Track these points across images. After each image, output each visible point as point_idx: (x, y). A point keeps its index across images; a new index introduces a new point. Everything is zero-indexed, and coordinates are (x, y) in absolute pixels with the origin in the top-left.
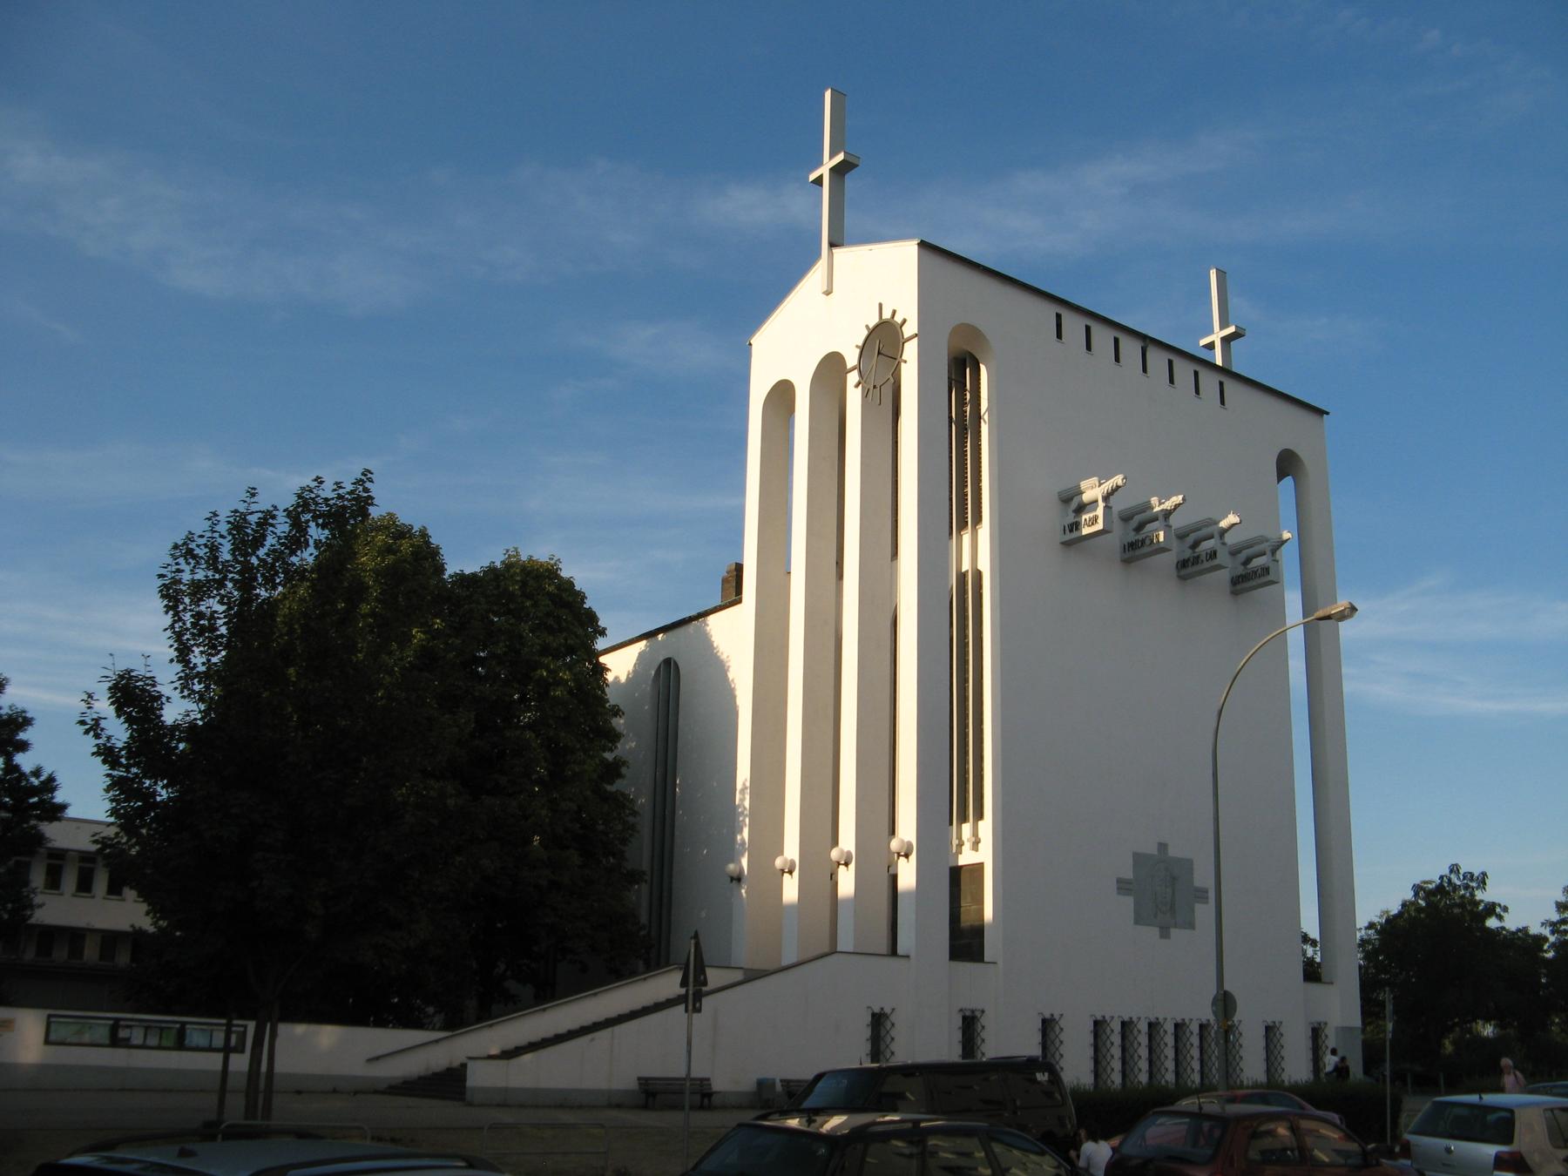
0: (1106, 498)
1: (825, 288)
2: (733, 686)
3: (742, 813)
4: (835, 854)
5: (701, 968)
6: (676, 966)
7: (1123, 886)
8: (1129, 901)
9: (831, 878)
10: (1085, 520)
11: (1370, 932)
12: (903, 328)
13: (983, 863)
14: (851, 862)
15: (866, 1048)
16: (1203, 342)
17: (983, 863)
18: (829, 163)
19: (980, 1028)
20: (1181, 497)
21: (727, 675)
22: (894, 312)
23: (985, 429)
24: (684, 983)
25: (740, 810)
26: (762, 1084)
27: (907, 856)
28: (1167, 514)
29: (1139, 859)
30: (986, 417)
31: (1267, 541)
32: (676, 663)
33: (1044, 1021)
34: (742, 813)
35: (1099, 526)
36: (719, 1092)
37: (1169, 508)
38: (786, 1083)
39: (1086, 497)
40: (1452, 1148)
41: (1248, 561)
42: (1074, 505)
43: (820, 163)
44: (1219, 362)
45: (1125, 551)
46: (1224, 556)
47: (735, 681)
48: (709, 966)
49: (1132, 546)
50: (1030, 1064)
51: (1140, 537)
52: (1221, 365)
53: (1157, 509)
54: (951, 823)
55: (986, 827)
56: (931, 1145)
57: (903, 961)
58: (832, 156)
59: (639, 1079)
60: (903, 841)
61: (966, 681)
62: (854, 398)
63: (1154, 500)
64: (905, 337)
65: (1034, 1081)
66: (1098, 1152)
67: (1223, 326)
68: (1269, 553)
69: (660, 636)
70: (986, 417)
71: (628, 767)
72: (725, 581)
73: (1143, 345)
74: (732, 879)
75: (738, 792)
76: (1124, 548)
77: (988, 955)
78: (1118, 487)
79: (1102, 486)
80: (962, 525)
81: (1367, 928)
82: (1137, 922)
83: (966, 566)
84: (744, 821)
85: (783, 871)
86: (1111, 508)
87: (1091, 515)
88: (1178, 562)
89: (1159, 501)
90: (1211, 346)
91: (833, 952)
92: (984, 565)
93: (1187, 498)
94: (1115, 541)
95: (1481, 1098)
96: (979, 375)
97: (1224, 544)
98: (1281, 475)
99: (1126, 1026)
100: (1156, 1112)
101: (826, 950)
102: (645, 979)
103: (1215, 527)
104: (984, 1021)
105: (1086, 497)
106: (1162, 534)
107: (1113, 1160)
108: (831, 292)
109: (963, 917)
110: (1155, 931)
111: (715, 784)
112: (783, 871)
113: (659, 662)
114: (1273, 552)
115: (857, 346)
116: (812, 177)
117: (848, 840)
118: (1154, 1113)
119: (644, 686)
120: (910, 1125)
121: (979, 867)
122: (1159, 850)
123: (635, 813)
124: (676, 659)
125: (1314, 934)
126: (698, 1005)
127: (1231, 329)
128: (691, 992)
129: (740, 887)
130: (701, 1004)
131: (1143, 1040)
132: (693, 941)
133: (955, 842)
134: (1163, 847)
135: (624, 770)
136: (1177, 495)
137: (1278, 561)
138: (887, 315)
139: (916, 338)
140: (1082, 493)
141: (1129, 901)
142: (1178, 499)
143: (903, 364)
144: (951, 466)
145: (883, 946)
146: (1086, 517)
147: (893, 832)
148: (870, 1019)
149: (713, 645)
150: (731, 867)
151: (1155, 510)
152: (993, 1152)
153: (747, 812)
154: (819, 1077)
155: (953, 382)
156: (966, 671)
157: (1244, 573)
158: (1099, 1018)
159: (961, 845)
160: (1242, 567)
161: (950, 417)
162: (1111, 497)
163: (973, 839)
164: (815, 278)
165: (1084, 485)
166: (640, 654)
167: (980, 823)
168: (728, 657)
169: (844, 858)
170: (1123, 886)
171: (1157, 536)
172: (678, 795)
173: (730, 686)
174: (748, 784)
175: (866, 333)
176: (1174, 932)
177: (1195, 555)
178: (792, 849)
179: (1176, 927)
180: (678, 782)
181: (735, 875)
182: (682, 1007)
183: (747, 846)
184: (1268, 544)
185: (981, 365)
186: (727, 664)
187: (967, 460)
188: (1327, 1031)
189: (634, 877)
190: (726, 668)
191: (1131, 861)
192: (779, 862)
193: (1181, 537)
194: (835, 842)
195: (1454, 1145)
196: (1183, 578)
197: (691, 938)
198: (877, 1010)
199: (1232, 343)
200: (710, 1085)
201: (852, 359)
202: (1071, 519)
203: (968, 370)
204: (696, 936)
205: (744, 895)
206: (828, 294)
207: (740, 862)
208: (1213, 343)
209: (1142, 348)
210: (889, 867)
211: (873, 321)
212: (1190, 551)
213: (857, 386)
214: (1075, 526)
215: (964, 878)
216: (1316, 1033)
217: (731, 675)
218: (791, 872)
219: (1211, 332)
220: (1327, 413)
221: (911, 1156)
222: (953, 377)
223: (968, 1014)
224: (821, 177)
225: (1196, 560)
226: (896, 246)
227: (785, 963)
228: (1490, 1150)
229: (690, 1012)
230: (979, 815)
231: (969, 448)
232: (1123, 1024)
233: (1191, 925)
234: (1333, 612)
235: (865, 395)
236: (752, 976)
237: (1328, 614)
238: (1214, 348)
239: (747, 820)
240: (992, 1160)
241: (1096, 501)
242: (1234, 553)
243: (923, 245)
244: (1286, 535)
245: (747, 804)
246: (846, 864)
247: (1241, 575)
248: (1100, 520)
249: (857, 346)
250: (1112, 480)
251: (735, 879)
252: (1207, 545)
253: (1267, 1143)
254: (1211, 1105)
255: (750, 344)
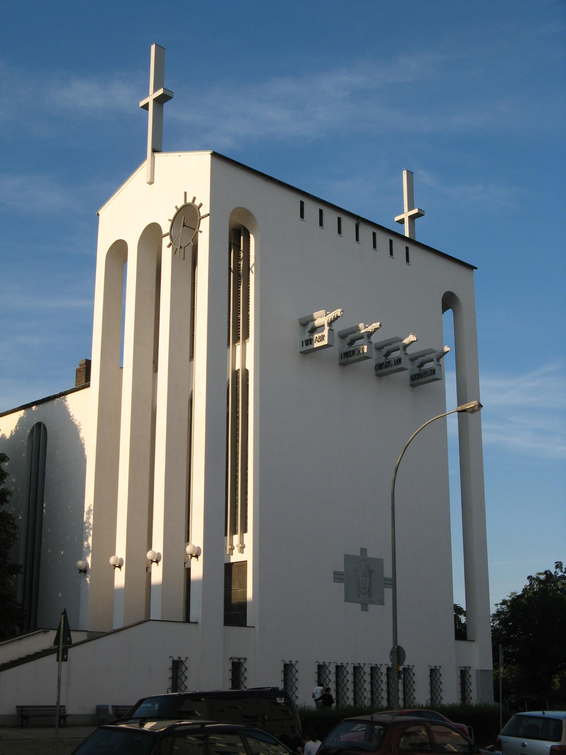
0: (330, 324)
1: (149, 180)
2: (83, 442)
3: (88, 527)
4: (149, 555)
5: (68, 632)
6: (41, 630)
7: (338, 577)
8: (341, 586)
9: (147, 571)
10: (316, 337)
11: (503, 606)
12: (200, 209)
13: (246, 561)
14: (160, 560)
15: (169, 684)
16: (397, 218)
17: (246, 561)
18: (153, 95)
19: (243, 670)
20: (378, 324)
21: (79, 435)
22: (194, 199)
23: (252, 277)
24: (57, 642)
25: (87, 525)
26: (100, 709)
27: (197, 556)
28: (369, 334)
29: (347, 558)
30: (253, 269)
31: (434, 352)
32: (44, 426)
33: (286, 665)
34: (88, 527)
35: (325, 342)
36: (71, 715)
37: (371, 331)
38: (115, 708)
39: (317, 323)
40: (526, 743)
41: (422, 364)
42: (309, 327)
43: (147, 95)
44: (407, 235)
45: (342, 358)
46: (405, 363)
47: (84, 439)
48: (72, 630)
49: (347, 355)
50: (274, 692)
51: (351, 349)
52: (408, 236)
53: (363, 331)
54: (226, 535)
55: (249, 537)
56: (211, 739)
57: (194, 626)
58: (155, 90)
59: (17, 707)
60: (194, 546)
61: (237, 441)
62: (167, 254)
63: (361, 325)
64: (201, 215)
65: (276, 703)
66: (313, 746)
67: (410, 209)
68: (435, 360)
69: (34, 407)
70: (253, 269)
71: (11, 496)
72: (78, 371)
73: (357, 223)
74: (81, 571)
75: (85, 513)
76: (341, 356)
77: (249, 623)
78: (338, 317)
79: (328, 316)
80: (237, 339)
81: (501, 604)
82: (346, 600)
83: (238, 366)
84: (89, 532)
85: (115, 566)
86: (333, 330)
87: (320, 335)
88: (376, 365)
89: (365, 326)
90: (402, 222)
91: (148, 620)
92: (250, 366)
93: (382, 324)
94: (335, 351)
95: (544, 713)
96: (249, 241)
97: (406, 354)
98: (445, 309)
99: (357, 669)
100: (346, 720)
101: (143, 619)
102: (21, 639)
103: (399, 343)
104: (246, 665)
105: (317, 323)
106: (366, 347)
107: (320, 749)
108: (153, 183)
109: (233, 597)
110: (359, 606)
111: (70, 507)
112: (115, 566)
113: (33, 425)
114: (438, 360)
115: (169, 220)
116: (142, 103)
117: (158, 546)
118: (345, 721)
119: (22, 441)
120: (199, 726)
121: (244, 564)
122: (361, 554)
123: (15, 527)
124: (44, 423)
125: (464, 606)
126: (65, 656)
127: (415, 211)
128: (61, 648)
129: (86, 577)
130: (67, 656)
131: (367, 678)
132: (63, 616)
133: (228, 547)
134: (364, 551)
135: (8, 498)
136: (376, 322)
137: (441, 365)
138: (189, 200)
139: (209, 217)
140: (314, 320)
141: (341, 586)
142: (376, 325)
143: (199, 233)
144: (230, 300)
145: (181, 618)
146: (316, 335)
147: (188, 540)
148: (171, 664)
149: (70, 415)
150: (80, 563)
151: (362, 332)
152: (248, 743)
153: (91, 527)
154: (141, 702)
155: (232, 245)
156: (237, 435)
157: (419, 373)
158: (288, 662)
159: (232, 549)
160: (418, 369)
161: (230, 268)
162: (333, 323)
163: (240, 545)
164: (142, 172)
165: (316, 315)
166: (20, 419)
167: (245, 534)
168: (80, 423)
169: (156, 558)
170: (338, 577)
171: (363, 349)
172: (44, 514)
173: (81, 442)
174: (92, 508)
175: (175, 211)
176: (370, 607)
177: (387, 361)
178: (121, 552)
179: (372, 603)
180: (44, 506)
181: (83, 568)
182: (55, 656)
183: (91, 549)
184: (434, 354)
185: (250, 234)
186: (79, 428)
187: (239, 323)
188: (470, 673)
189: (14, 569)
190: (78, 430)
191: (342, 562)
192: (112, 560)
193: (379, 348)
194: (150, 547)
195: (527, 741)
196: (379, 376)
197: (62, 614)
198: (176, 659)
199: (415, 220)
200: (65, 710)
201: (166, 228)
202: (307, 337)
203: (242, 237)
204: (65, 613)
205: (89, 582)
206: (150, 184)
207: (86, 560)
208: (403, 219)
209: (356, 224)
210: (185, 563)
211: (181, 204)
212: (384, 358)
213: (169, 246)
214: (310, 342)
215: (234, 570)
216: (464, 674)
217: (81, 435)
218: (120, 567)
219: (402, 212)
220: (476, 268)
221: (200, 745)
222: (232, 242)
223: (236, 660)
224: (147, 105)
225: (388, 364)
226: (197, 155)
227: (115, 627)
228: (548, 744)
229: (60, 661)
230: (245, 530)
231: (241, 289)
232: (337, 667)
233: (382, 603)
234: (467, 407)
235: (174, 253)
236: (94, 636)
237: (464, 409)
238: (404, 223)
239: (91, 532)
240: (247, 748)
241: (324, 326)
242: (413, 359)
243: (214, 155)
244: (446, 349)
245: (91, 521)
246: (157, 562)
247: (417, 374)
248: (326, 338)
249: (169, 220)
250: (334, 312)
251: (82, 571)
252: (395, 355)
253: (413, 739)
254: (386, 717)
255: (98, 215)
